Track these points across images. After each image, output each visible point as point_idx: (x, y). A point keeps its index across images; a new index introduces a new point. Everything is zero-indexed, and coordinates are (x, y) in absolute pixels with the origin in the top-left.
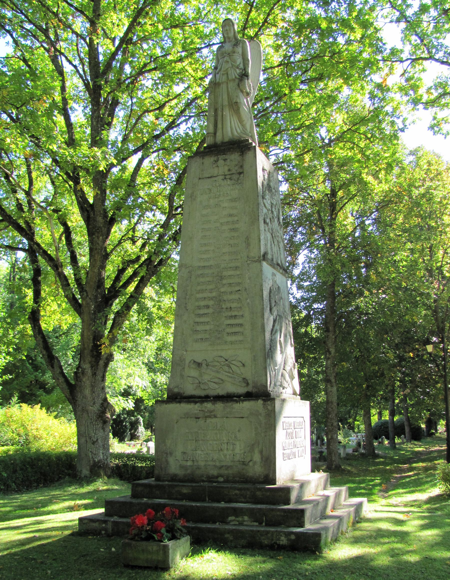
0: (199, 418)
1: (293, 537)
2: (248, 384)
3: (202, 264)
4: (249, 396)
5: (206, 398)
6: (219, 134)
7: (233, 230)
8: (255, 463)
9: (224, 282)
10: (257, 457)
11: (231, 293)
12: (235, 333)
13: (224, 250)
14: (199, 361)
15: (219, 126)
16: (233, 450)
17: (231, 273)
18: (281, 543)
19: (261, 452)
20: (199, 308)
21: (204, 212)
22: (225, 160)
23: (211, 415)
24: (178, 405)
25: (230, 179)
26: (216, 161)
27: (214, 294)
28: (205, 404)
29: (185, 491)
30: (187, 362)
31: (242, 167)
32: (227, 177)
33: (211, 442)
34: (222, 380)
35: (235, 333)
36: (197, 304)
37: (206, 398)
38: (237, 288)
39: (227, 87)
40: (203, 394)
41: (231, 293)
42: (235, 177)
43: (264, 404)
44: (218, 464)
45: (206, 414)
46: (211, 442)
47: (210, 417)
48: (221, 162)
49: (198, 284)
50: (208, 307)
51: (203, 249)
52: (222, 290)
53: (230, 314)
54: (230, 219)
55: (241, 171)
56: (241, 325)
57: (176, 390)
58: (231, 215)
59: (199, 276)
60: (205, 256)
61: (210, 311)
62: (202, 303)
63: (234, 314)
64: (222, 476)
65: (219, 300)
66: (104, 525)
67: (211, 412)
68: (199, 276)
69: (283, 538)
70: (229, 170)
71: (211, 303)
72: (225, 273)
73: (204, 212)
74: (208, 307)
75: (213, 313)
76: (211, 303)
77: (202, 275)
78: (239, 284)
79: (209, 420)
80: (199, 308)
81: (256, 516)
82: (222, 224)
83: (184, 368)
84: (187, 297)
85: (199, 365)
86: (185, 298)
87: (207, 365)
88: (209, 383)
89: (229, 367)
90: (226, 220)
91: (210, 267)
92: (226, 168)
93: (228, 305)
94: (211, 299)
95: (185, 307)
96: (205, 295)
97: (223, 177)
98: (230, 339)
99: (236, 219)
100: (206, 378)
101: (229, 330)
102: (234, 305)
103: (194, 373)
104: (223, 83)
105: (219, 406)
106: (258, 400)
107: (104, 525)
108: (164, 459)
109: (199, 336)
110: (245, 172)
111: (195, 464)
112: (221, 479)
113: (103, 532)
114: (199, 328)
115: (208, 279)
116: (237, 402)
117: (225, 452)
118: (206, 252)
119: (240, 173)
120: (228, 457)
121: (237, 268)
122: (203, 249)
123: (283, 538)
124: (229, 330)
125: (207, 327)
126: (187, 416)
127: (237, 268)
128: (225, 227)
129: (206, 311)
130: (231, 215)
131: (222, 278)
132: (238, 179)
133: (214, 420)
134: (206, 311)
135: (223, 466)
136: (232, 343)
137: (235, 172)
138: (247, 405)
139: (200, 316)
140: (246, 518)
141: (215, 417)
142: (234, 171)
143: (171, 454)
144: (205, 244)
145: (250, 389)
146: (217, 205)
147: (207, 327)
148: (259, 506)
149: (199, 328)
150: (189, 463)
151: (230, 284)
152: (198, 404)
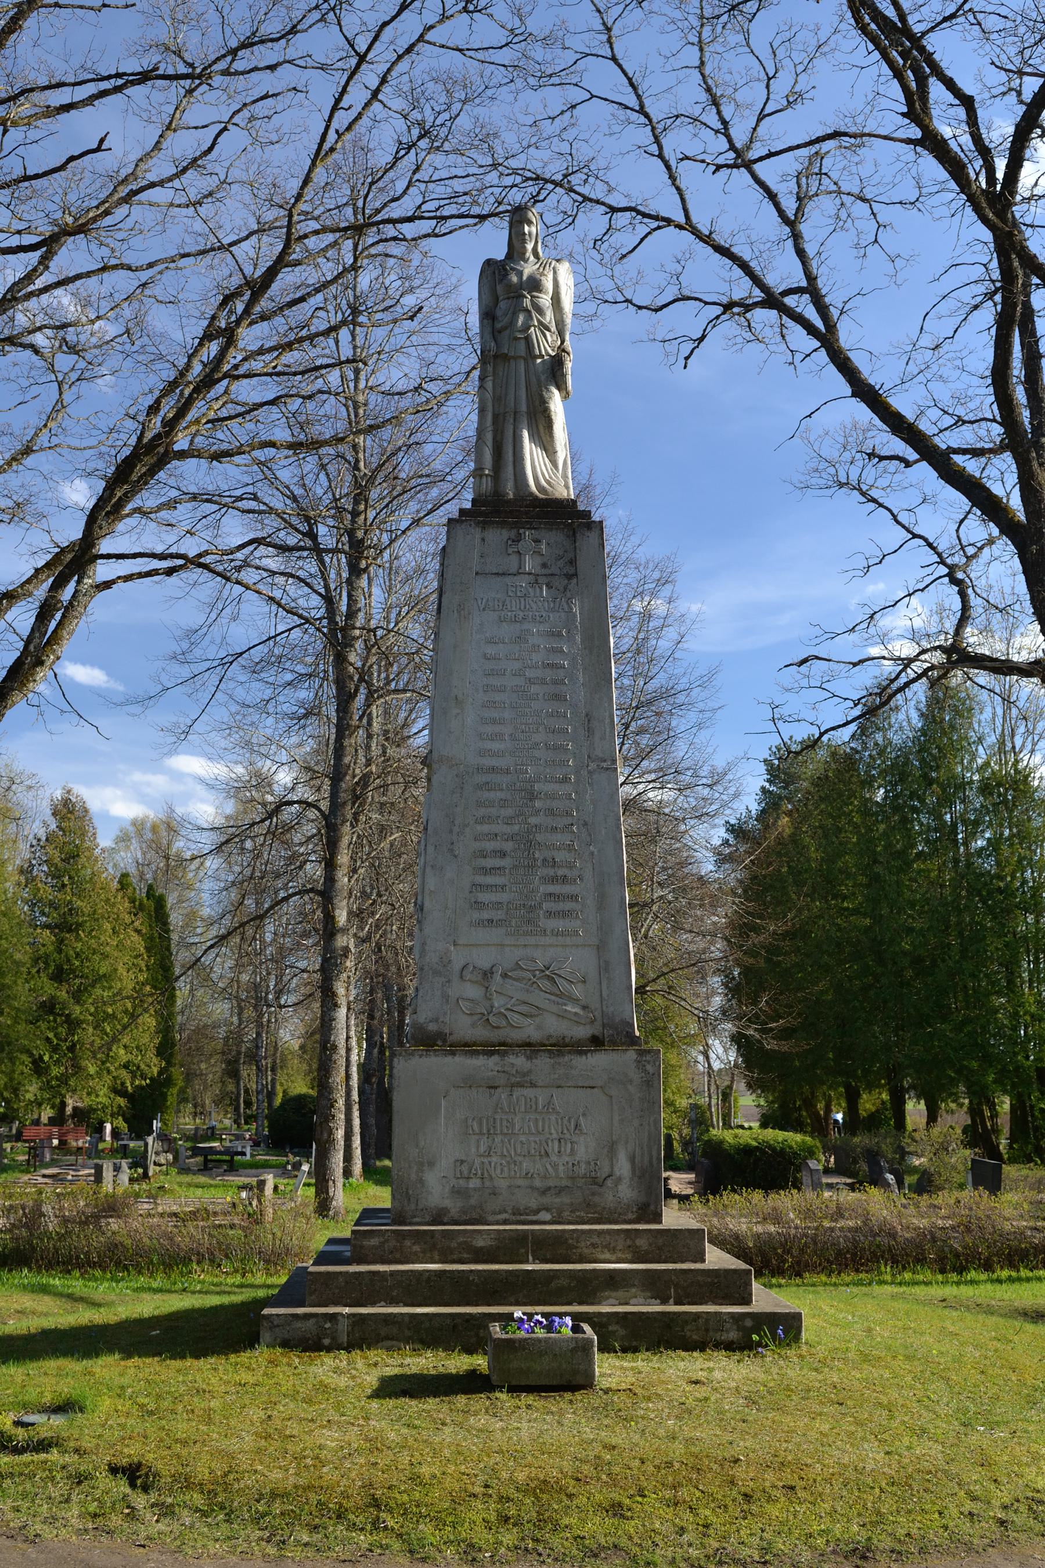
0: (496, 1088)
3: (488, 762)
4: (597, 1042)
8: (620, 1179)
9: (538, 804)
13: (538, 738)
16: (573, 1152)
17: (549, 787)
21: (491, 650)
23: (523, 1081)
26: (518, 539)
28: (511, 1059)
30: (457, 967)
31: (573, 562)
33: (523, 1138)
36: (477, 845)
40: (494, 1036)
41: (554, 829)
42: (560, 582)
44: (537, 1183)
45: (513, 1080)
46: (523, 1138)
47: (520, 1085)
49: (480, 804)
50: (503, 854)
51: (489, 729)
52: (533, 820)
53: (551, 872)
55: (572, 571)
56: (573, 898)
59: (479, 787)
60: (495, 746)
61: (506, 862)
62: (490, 845)
64: (547, 1210)
65: (527, 842)
67: (525, 1075)
68: (479, 787)
70: (544, 565)
71: (508, 846)
72: (539, 838)
74: (503, 854)
75: (515, 867)
76: (508, 846)
77: (486, 786)
79: (518, 1092)
82: (531, 681)
83: (449, 981)
84: (456, 829)
86: (451, 831)
87: (505, 976)
88: (508, 1014)
90: (538, 673)
91: (508, 772)
93: (548, 854)
94: (511, 838)
95: (451, 850)
96: (495, 828)
98: (552, 924)
102: (560, 856)
104: (516, 358)
105: (543, 1063)
108: (413, 1177)
109: (485, 915)
110: (581, 576)
111: (487, 1184)
114: (485, 897)
115: (500, 795)
116: (581, 1053)
117: (554, 1158)
118: (494, 737)
119: (570, 577)
120: (561, 1168)
122: (489, 729)
125: (504, 897)
126: (469, 1082)
128: (534, 689)
129: (498, 862)
131: (532, 796)
132: (565, 589)
133: (529, 1092)
134: (498, 862)
135: (549, 1188)
137: (557, 571)
138: (600, 1061)
139: (485, 871)
141: (533, 1085)
142: (554, 569)
144: (494, 721)
146: (520, 639)
147: (504, 897)
148: (508, 1227)
149: (485, 897)
152: (496, 1058)
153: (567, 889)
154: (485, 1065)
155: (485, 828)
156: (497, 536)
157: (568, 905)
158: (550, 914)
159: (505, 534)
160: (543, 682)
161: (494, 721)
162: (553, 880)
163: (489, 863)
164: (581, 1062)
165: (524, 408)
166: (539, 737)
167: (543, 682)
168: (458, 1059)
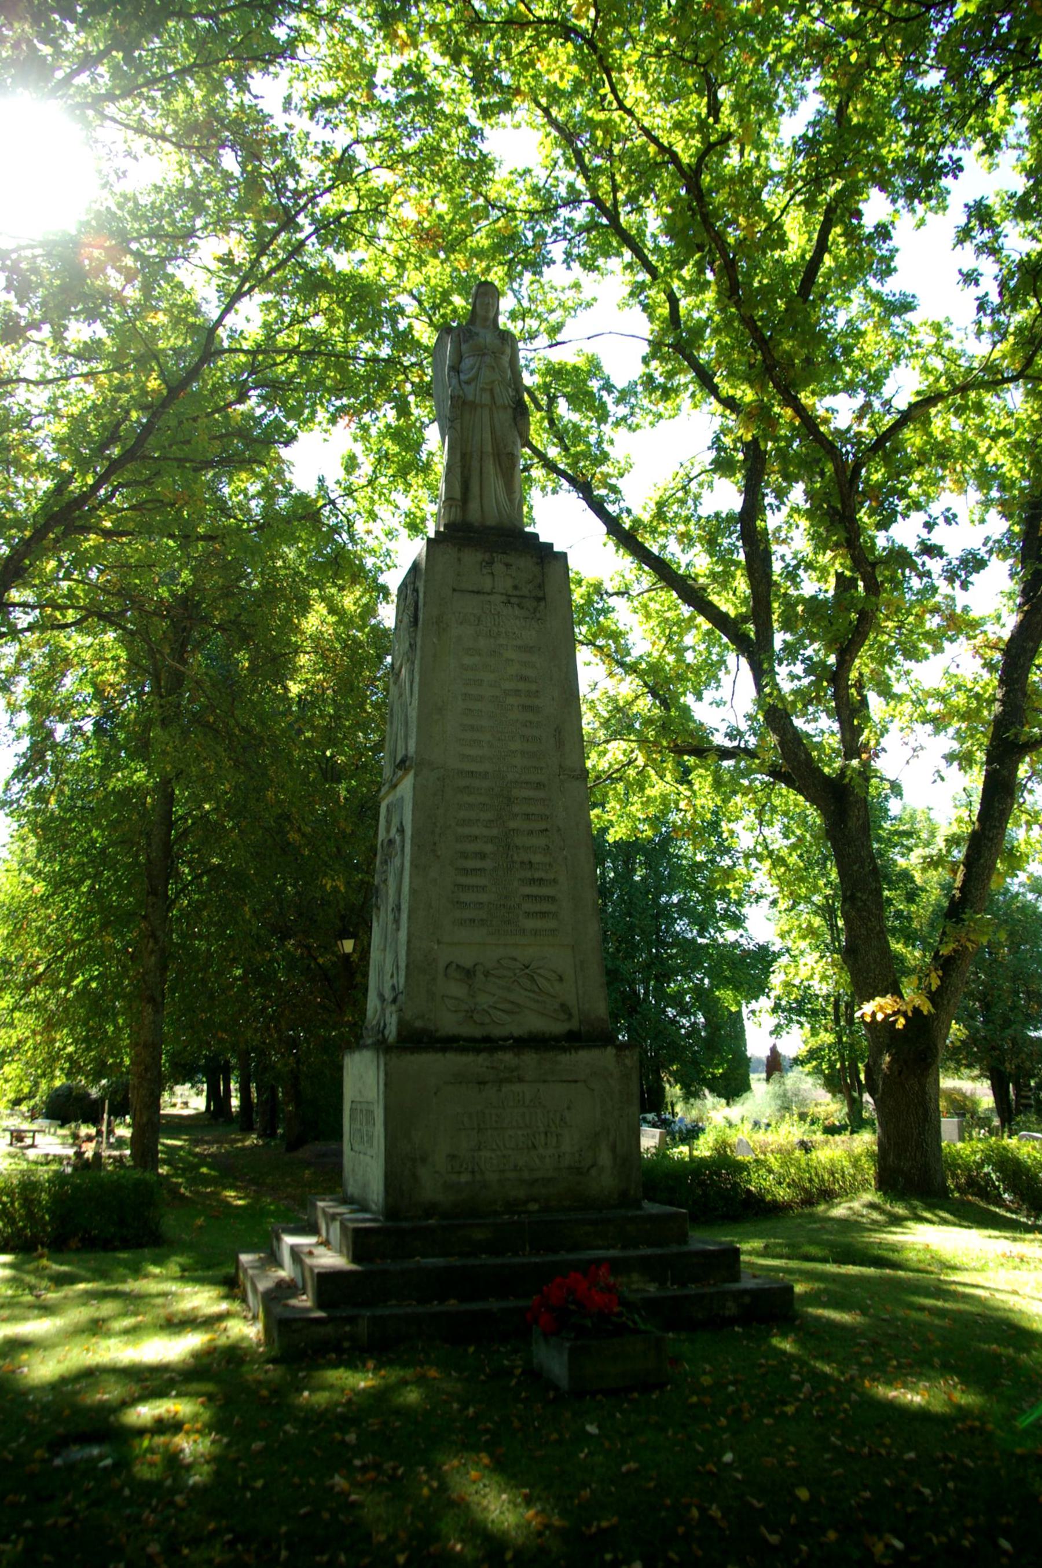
0: (484, 1083)
1: (747, 1300)
2: (570, 1016)
5: (487, 1044)
6: (474, 506)
7: (527, 708)
9: (516, 809)
10: (605, 1158)
11: (531, 833)
12: (543, 915)
14: (468, 964)
15: (475, 489)
17: (531, 793)
18: (727, 1313)
19: (613, 1148)
20: (464, 855)
21: (468, 661)
22: (508, 565)
24: (439, 1056)
25: (520, 606)
26: (491, 563)
27: (495, 832)
28: (500, 1055)
29: (479, 1235)
30: (442, 965)
31: (541, 586)
32: (513, 600)
34: (518, 1005)
35: (543, 915)
37: (487, 1044)
38: (543, 825)
39: (492, 418)
40: (478, 1032)
41: (531, 833)
43: (617, 1056)
44: (526, 1175)
47: (509, 1081)
48: (498, 568)
50: (483, 856)
52: (512, 825)
53: (529, 874)
54: (522, 686)
56: (552, 899)
57: (419, 1024)
58: (523, 679)
60: (473, 752)
61: (488, 864)
63: (537, 875)
66: (347, 1328)
69: (730, 1304)
70: (515, 587)
71: (489, 848)
72: (515, 792)
73: (468, 661)
74: (483, 856)
76: (489, 848)
78: (544, 818)
80: (464, 855)
81: (650, 1267)
85: (469, 974)
87: (487, 974)
89: (533, 980)
91: (485, 775)
92: (509, 583)
96: (476, 831)
97: (504, 598)
98: (530, 924)
99: (534, 687)
100: (484, 1000)
101: (528, 906)
102: (537, 858)
103: (457, 989)
104: (482, 406)
105: (529, 1059)
106: (605, 1046)
107: (347, 1328)
112: (534, 1207)
113: (346, 1344)
114: (467, 897)
116: (564, 1050)
119: (540, 599)
121: (539, 785)
123: (730, 1304)
124: (528, 906)
125: (484, 898)
127: (539, 785)
128: (511, 700)
130: (523, 679)
132: (535, 610)
133: (517, 1087)
136: (536, 932)
138: (585, 1058)
139: (466, 872)
140: (635, 1276)
141: (521, 1080)
143: (424, 1160)
144: (473, 728)
145: (574, 1025)
147: (484, 898)
149: (467, 897)
150: (464, 1178)
151: (528, 816)
152: (483, 1056)
153: (544, 891)
154: (475, 1062)
155: (467, 830)
156: (471, 558)
157: (545, 907)
158: (528, 914)
159: (479, 556)
160: (517, 692)
161: (473, 728)
162: (533, 881)
163: (471, 864)
164: (565, 1059)
165: (489, 448)
166: (516, 746)
167: (517, 692)
168: (450, 1056)
